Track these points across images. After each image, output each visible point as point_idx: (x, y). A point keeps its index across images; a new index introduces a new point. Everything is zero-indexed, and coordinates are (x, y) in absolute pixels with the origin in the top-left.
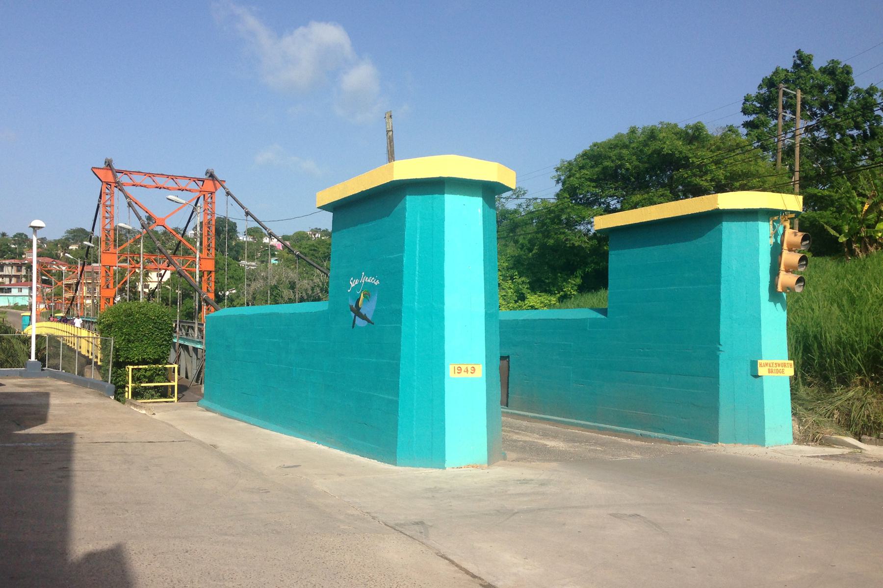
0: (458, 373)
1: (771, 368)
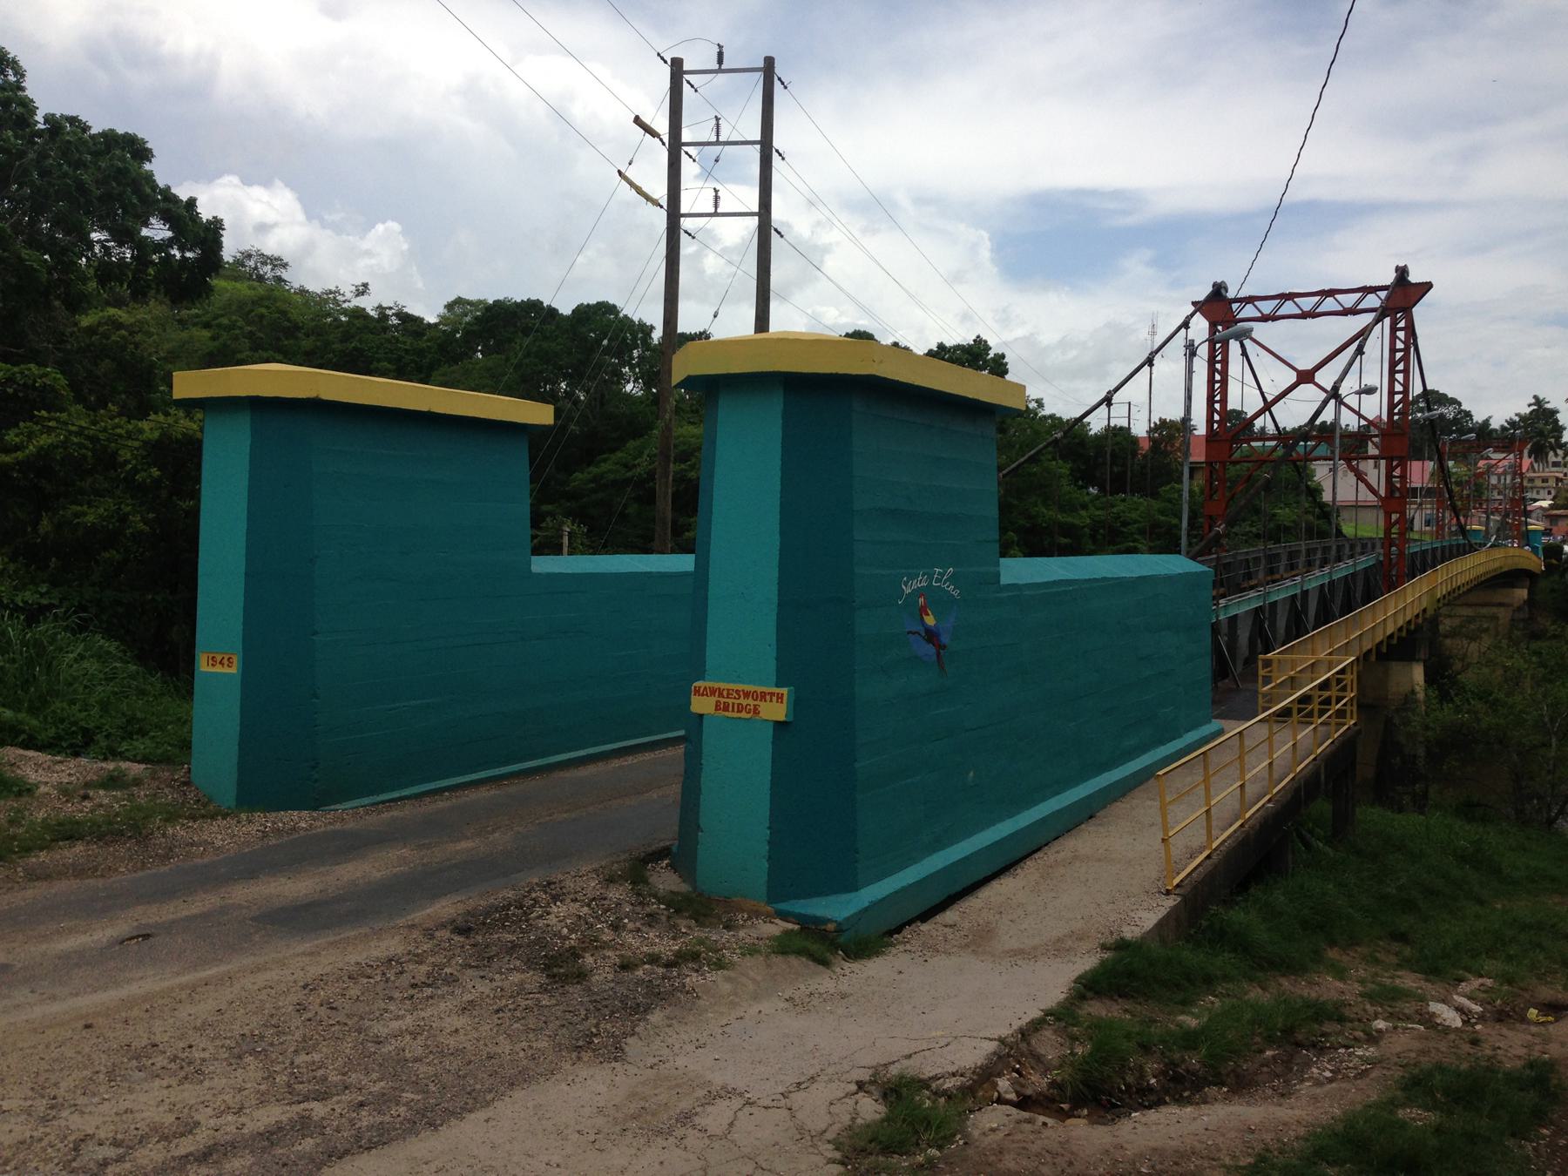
1: (722, 700)
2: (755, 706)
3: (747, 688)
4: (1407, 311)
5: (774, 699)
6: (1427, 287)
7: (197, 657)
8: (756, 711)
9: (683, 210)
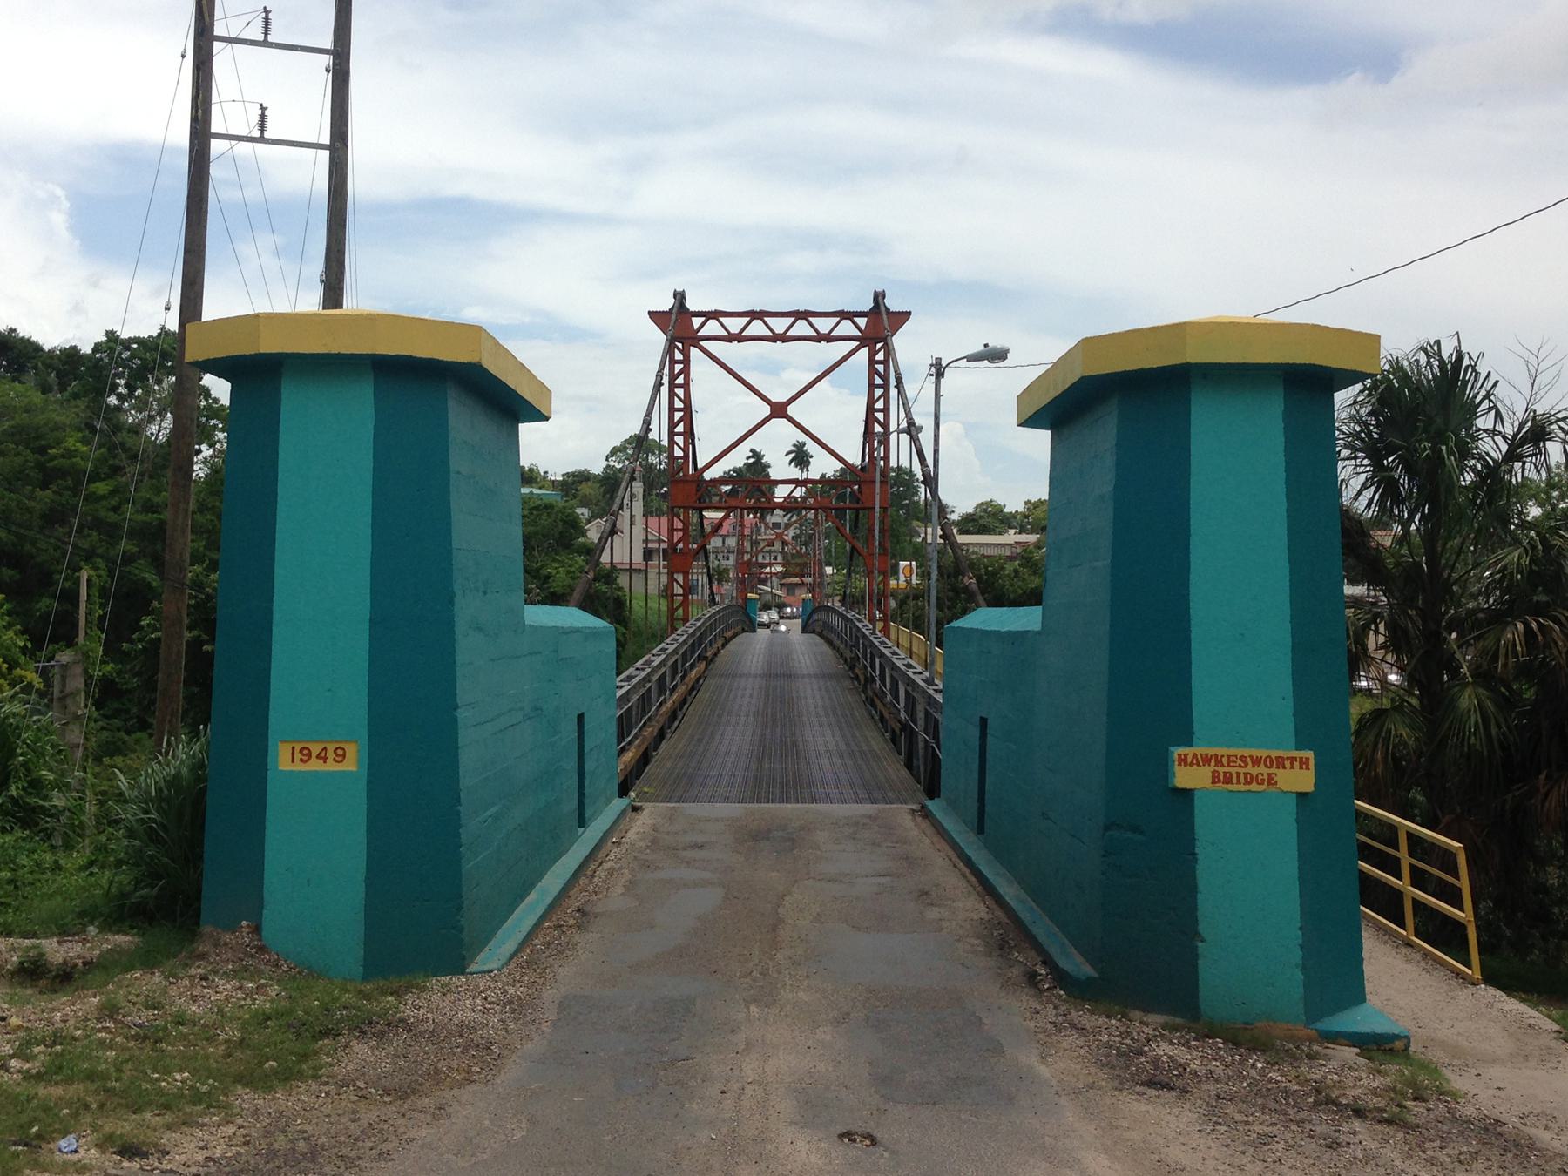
0: (301, 760)
1: (1221, 770)
2: (1269, 775)
3: (1256, 753)
4: (886, 341)
5: (1297, 764)
6: (904, 316)
7: (271, 749)
8: (1271, 781)
9: (215, 127)
